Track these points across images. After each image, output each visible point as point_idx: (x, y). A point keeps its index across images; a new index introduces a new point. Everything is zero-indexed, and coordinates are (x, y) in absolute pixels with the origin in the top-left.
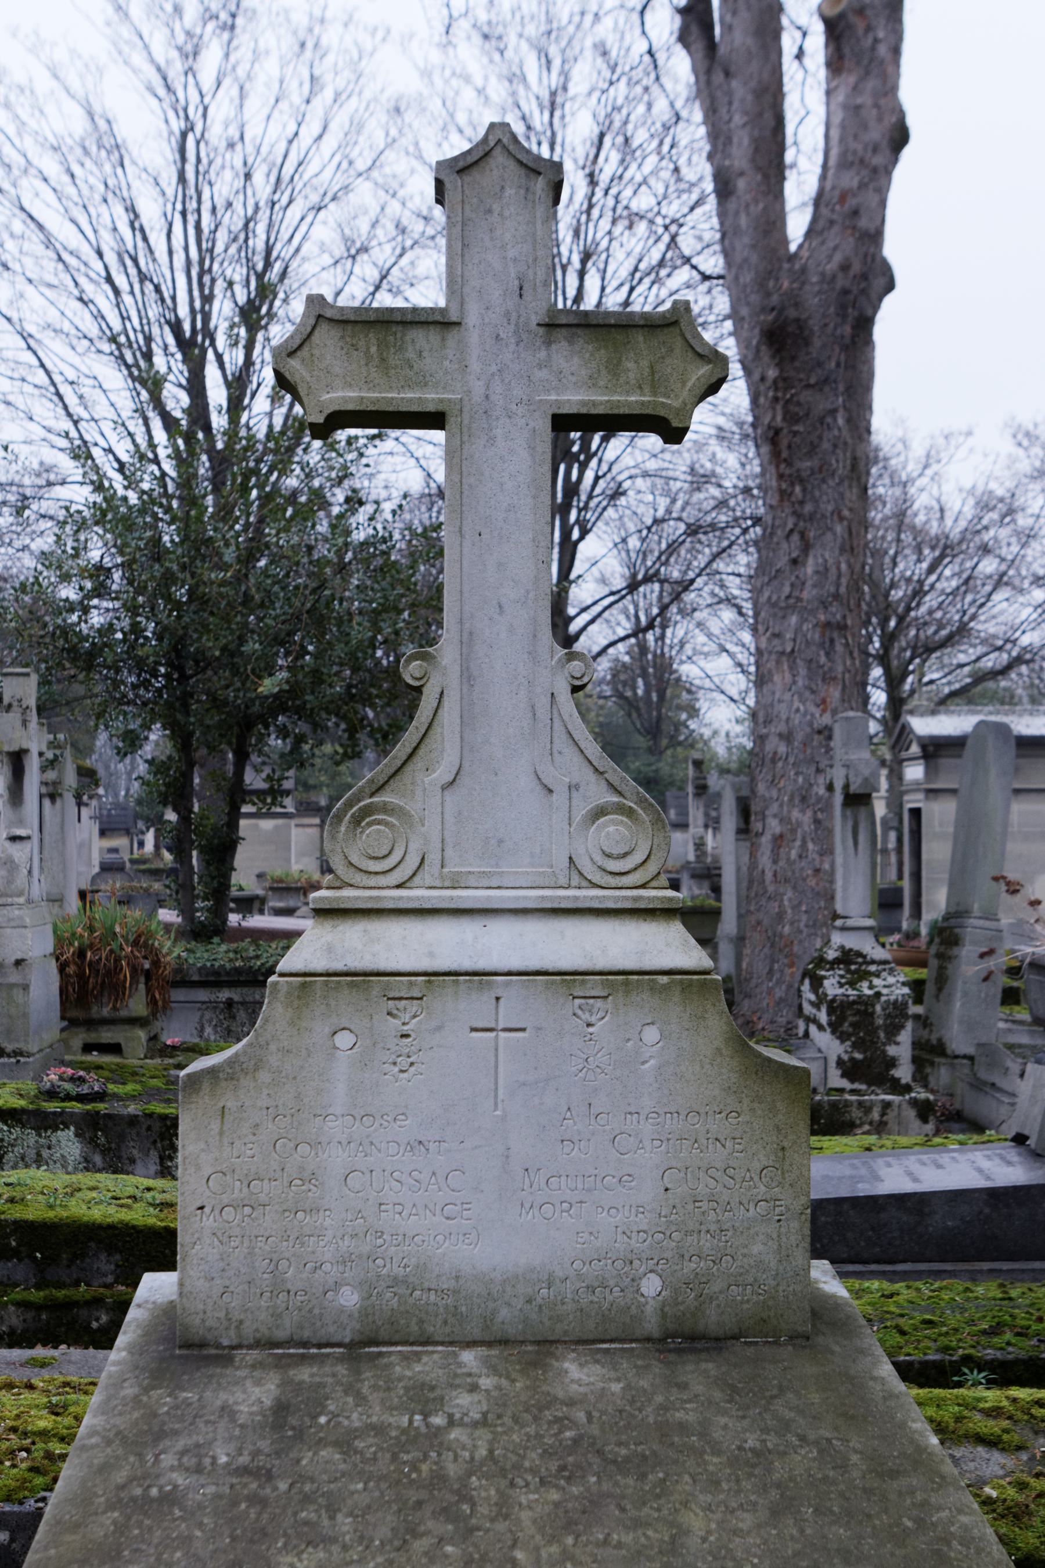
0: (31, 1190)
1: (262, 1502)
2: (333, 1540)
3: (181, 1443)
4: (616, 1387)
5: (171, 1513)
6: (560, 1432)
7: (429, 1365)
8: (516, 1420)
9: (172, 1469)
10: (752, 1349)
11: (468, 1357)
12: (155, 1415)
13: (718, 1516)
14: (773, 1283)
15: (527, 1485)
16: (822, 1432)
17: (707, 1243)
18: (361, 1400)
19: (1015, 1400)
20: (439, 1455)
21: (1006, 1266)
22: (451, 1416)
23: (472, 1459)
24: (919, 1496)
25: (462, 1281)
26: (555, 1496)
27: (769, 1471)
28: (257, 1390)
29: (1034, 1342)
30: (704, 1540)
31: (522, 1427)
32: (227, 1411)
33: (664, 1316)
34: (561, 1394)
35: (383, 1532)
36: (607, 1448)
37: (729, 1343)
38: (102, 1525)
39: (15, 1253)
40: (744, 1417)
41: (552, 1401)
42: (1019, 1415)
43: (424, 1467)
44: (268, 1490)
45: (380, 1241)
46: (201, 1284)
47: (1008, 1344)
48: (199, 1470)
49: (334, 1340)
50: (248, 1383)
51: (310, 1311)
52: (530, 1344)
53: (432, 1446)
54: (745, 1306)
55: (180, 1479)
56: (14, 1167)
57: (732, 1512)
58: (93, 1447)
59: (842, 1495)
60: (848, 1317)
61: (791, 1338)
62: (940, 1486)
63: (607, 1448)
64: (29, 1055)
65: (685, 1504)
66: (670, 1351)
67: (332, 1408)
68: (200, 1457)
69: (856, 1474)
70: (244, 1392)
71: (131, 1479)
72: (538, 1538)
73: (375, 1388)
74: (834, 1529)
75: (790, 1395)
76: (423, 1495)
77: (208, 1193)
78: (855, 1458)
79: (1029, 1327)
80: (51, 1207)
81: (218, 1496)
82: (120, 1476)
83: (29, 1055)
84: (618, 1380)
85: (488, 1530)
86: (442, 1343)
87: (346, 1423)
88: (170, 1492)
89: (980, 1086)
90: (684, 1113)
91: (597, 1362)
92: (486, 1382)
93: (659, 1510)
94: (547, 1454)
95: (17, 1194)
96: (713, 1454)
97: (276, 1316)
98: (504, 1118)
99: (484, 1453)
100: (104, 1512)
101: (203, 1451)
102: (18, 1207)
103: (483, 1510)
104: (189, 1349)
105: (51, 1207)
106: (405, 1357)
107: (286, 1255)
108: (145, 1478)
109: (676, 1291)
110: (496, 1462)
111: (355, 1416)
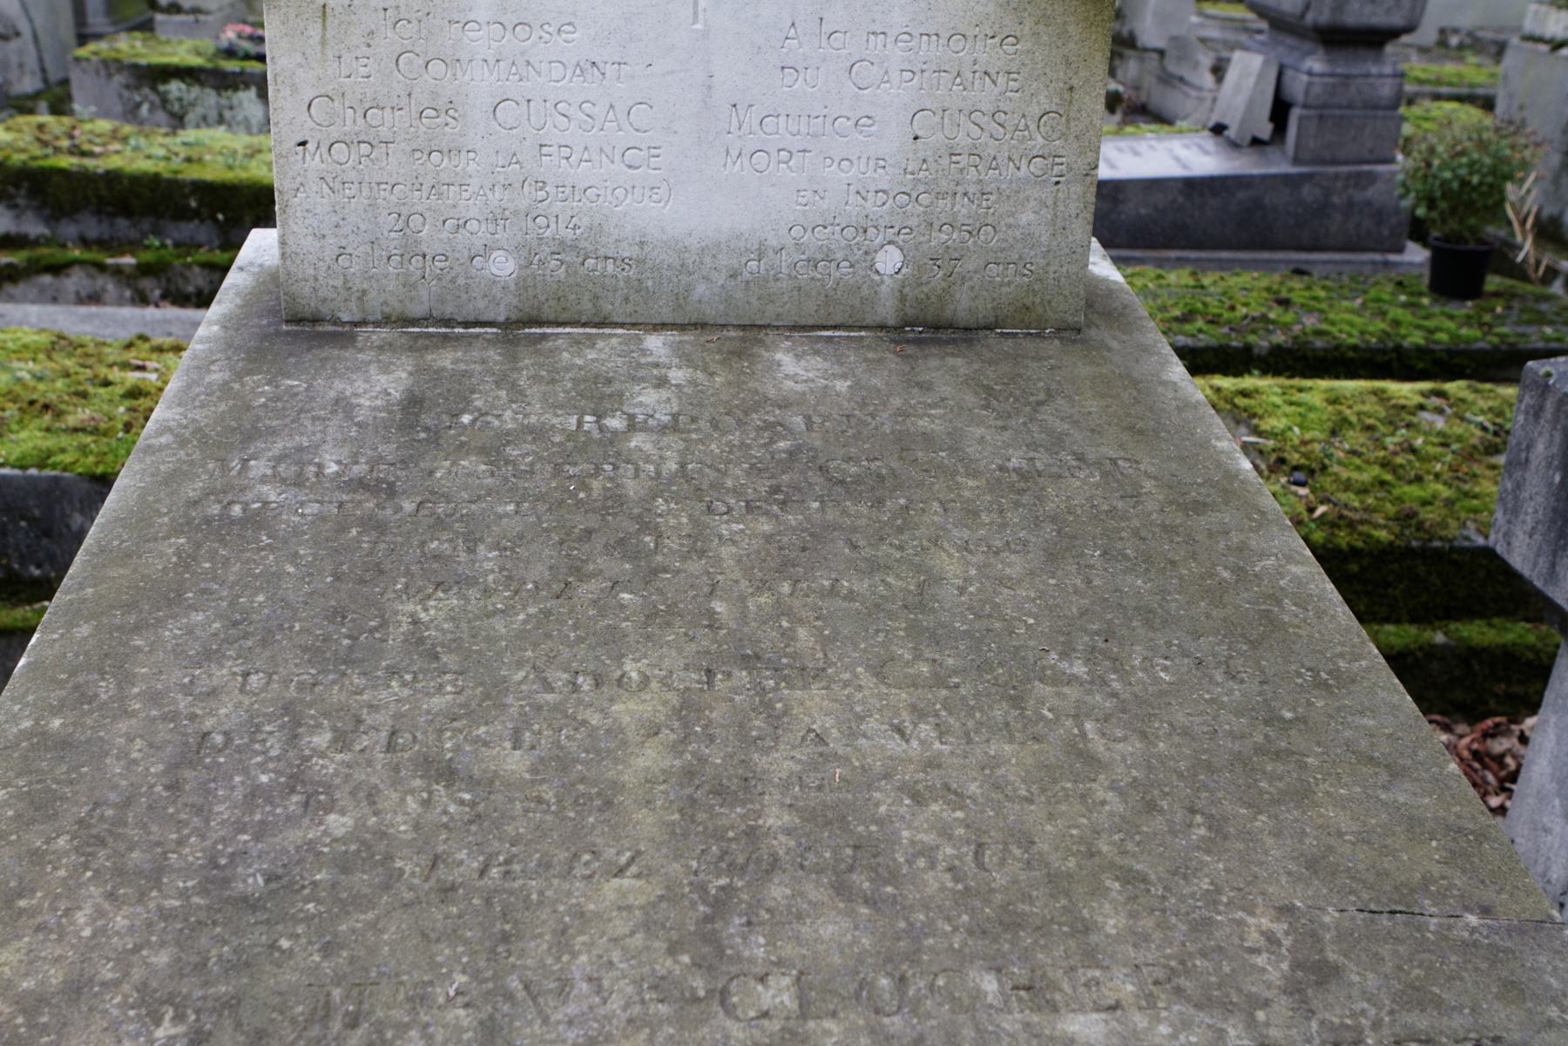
0: (210, 150)
1: (381, 527)
2: (471, 581)
3: (279, 446)
4: (842, 386)
5: (257, 540)
6: (772, 442)
7: (605, 352)
8: (715, 424)
9: (264, 480)
10: (1010, 342)
11: (655, 343)
12: (248, 408)
13: (978, 558)
14: (1042, 262)
15: (729, 511)
16: (1104, 449)
17: (963, 208)
18: (517, 394)
19: (1218, 390)
20: (616, 468)
21: (1193, 254)
22: (631, 417)
23: (658, 473)
24: (1235, 538)
25: (647, 249)
26: (766, 527)
27: (1040, 499)
28: (383, 378)
29: (1225, 330)
30: (962, 590)
31: (725, 434)
32: (343, 405)
33: (903, 299)
34: (772, 393)
35: (539, 571)
36: (832, 465)
37: (981, 333)
38: (161, 555)
39: (195, 214)
40: (1004, 428)
41: (761, 402)
42: (1222, 404)
43: (596, 485)
44: (389, 512)
45: (542, 194)
46: (308, 243)
47: (1200, 331)
48: (299, 482)
49: (485, 318)
50: (373, 369)
51: (453, 281)
52: (732, 326)
53: (606, 456)
54: (1005, 289)
55: (271, 493)
56: (198, 126)
57: (997, 553)
58: (161, 448)
59: (1136, 532)
60: (1125, 307)
61: (1058, 330)
62: (1261, 525)
63: (832, 465)
64: (207, 13)
65: (935, 541)
66: (908, 342)
67: (479, 403)
68: (302, 464)
69: (1151, 505)
70: (367, 381)
71: (207, 494)
72: (744, 583)
73: (536, 379)
74: (1129, 579)
75: (1060, 401)
76: (593, 521)
77: (310, 124)
78: (1148, 485)
79: (1220, 315)
80: (230, 168)
81: (321, 518)
82: (192, 490)
83: (207, 13)
84: (844, 376)
85: (678, 572)
86: (622, 325)
87: (496, 423)
88: (258, 512)
89: (1167, 79)
90: (945, 35)
91: (817, 353)
92: (677, 375)
93: (901, 548)
94: (755, 470)
95: (194, 153)
96: (968, 475)
97: (410, 286)
98: (705, 34)
99: (674, 467)
100: (165, 538)
101: (306, 457)
102: (195, 167)
103: (672, 544)
104: (301, 326)
105: (230, 168)
106: (576, 342)
107: (419, 208)
108: (225, 492)
109: (920, 268)
110: (689, 480)
111: (508, 414)
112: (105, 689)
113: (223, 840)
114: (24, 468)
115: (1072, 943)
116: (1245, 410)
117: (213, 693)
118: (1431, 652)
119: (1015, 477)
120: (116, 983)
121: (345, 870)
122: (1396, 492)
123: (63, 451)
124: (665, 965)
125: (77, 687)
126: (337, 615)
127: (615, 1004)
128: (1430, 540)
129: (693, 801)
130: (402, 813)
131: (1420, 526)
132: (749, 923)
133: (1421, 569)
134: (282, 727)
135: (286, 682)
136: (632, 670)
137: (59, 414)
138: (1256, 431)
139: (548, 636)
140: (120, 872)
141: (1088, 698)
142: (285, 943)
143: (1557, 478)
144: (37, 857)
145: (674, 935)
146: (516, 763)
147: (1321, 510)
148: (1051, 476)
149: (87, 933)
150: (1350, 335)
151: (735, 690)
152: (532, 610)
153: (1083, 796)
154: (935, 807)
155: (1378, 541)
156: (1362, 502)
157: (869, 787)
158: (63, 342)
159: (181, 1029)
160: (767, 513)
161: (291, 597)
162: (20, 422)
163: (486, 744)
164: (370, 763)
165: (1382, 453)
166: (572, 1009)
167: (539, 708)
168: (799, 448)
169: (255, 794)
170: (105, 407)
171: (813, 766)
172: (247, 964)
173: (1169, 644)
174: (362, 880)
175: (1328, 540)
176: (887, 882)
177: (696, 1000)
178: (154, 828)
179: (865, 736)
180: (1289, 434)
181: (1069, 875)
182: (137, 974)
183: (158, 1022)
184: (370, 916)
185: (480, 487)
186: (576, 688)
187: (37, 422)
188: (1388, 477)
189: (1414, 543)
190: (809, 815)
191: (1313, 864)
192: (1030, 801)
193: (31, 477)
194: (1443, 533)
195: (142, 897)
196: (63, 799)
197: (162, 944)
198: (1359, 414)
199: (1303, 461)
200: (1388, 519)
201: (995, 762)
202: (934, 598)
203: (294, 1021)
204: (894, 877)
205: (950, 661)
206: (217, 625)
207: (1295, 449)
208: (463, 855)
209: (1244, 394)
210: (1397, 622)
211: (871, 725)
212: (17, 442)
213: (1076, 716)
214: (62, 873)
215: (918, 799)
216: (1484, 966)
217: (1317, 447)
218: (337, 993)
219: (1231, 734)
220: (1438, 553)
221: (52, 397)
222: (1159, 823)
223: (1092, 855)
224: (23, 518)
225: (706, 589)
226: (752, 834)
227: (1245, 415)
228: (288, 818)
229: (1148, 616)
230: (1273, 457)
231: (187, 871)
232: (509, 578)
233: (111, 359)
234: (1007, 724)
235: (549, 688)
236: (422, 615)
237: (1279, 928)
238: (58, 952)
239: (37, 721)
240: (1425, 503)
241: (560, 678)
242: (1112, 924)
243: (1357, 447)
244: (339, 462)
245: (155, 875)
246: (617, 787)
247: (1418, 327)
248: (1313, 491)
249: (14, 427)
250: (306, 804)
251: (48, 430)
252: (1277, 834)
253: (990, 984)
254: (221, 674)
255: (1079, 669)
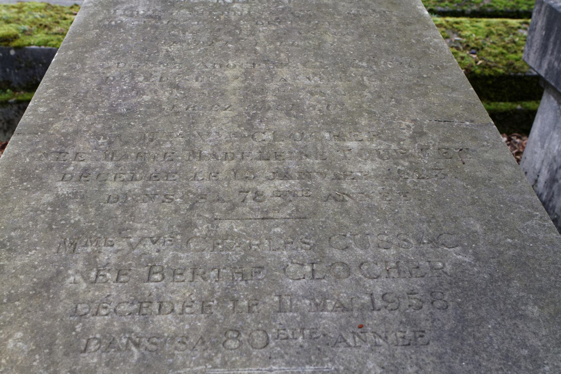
1: (157, 28)
2: (184, 41)
3: (125, 6)
6: (277, 6)
9: (121, 15)
15: (263, 24)
20: (228, 13)
23: (242, 14)
24: (419, 32)
26: (274, 28)
29: (455, 5)
30: (332, 45)
31: (263, 4)
35: (204, 39)
40: (351, 3)
43: (222, 17)
44: (159, 24)
47: (446, 5)
48: (132, 16)
53: (225, 10)
55: (124, 19)
58: (89, 7)
68: (132, 11)
71: (104, 19)
74: (383, 42)
76: (221, 26)
78: (394, 18)
81: (139, 25)
82: (100, 18)
93: (314, 34)
94: (271, 13)
96: (338, 15)
99: (246, 12)
101: (133, 9)
112: (78, 66)
113: (114, 101)
114: (40, 46)
115: (352, 127)
116: (457, 28)
117: (109, 68)
118: (516, 112)
119: (352, 16)
120: (87, 131)
121: (148, 108)
122: (507, 56)
123: (52, 40)
124: (237, 130)
125: (70, 66)
126: (144, 49)
127: (223, 137)
128: (517, 73)
129: (247, 94)
130: (164, 96)
131: (514, 68)
132: (261, 121)
133: (514, 83)
134: (129, 76)
135: (130, 65)
136: (231, 63)
137: (50, 29)
138: (460, 36)
139: (207, 55)
140: (86, 107)
141: (366, 71)
142: (132, 123)
143: (544, 33)
144: (63, 104)
145: (240, 123)
146: (197, 85)
147: (480, 62)
148: (364, 15)
149: (78, 120)
150: (500, 6)
151: (261, 68)
152: (202, 49)
153: (360, 95)
154: (317, 96)
155: (499, 73)
156: (495, 60)
157: (298, 91)
158: (49, 7)
159: (105, 141)
160: (274, 25)
161: (130, 44)
162: (37, 31)
163: (188, 80)
164: (155, 84)
165: (503, 43)
166: (211, 138)
167: (204, 72)
168: (286, 8)
169: (122, 91)
170: (65, 26)
171: (283, 86)
172: (122, 128)
173: (393, 58)
174: (153, 110)
175: (481, 72)
176: (301, 113)
177: (245, 137)
178: (95, 98)
179: (298, 80)
180: (471, 37)
181: (353, 112)
182: (93, 129)
183: (99, 139)
184: (156, 118)
185: (187, 17)
186: (214, 68)
187: (43, 31)
188: (505, 51)
189: (512, 74)
190: (280, 98)
191: (424, 111)
192: (345, 95)
193: (42, 49)
194: (522, 70)
195: (93, 113)
196: (69, 91)
197: (99, 123)
198: (497, 30)
199: (475, 46)
200: (503, 65)
201: (336, 86)
202: (323, 47)
203: (135, 140)
204: (303, 112)
205: (326, 62)
206: (109, 51)
207: (473, 42)
208: (181, 105)
209: (457, 23)
210: (505, 101)
211: (301, 77)
212: (37, 38)
213: (361, 76)
214: (70, 107)
215: (312, 94)
216: (468, 133)
217: (480, 41)
218: (147, 135)
219: (407, 81)
220: (520, 78)
221: (47, 23)
222: (381, 100)
223: (360, 107)
224: (40, 63)
225: (254, 44)
226: (263, 101)
227: (456, 30)
228: (132, 96)
229: (387, 51)
230: (465, 45)
231: (104, 108)
232: (195, 41)
233: (66, 11)
234: (341, 77)
235: (206, 67)
236: (169, 50)
237: (411, 124)
238: (71, 124)
239: (59, 74)
240: (517, 60)
241: (210, 65)
242: (364, 122)
243: (495, 41)
244: (144, 11)
245: (96, 108)
246: (226, 90)
247: (526, 4)
248: (478, 56)
249: (36, 33)
250: (137, 94)
251: (47, 34)
252: (415, 103)
253: (327, 135)
254: (111, 63)
255: (364, 64)
